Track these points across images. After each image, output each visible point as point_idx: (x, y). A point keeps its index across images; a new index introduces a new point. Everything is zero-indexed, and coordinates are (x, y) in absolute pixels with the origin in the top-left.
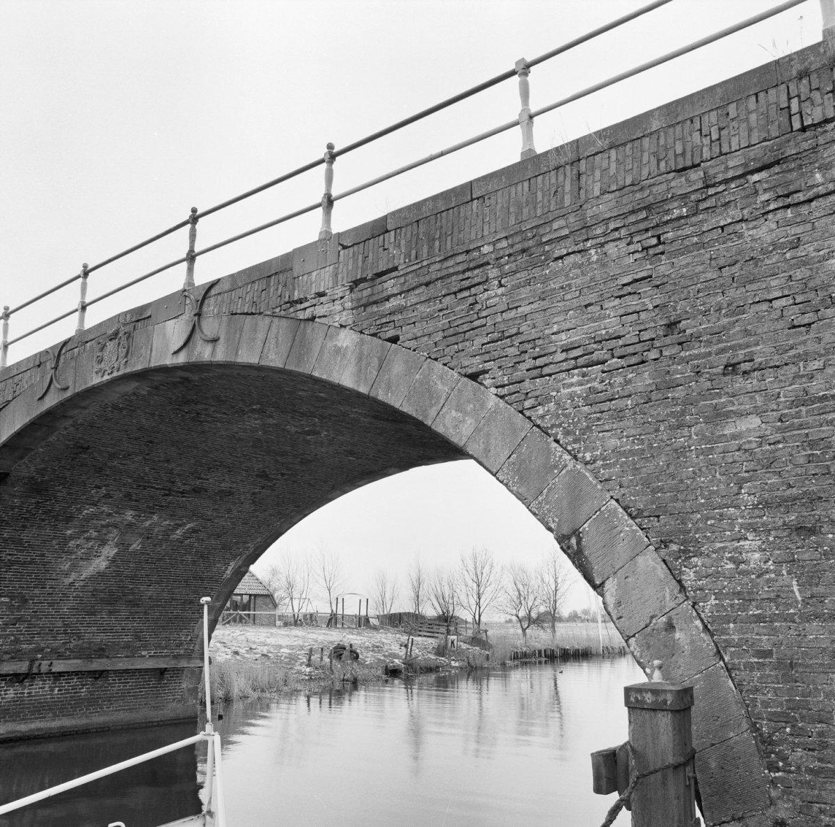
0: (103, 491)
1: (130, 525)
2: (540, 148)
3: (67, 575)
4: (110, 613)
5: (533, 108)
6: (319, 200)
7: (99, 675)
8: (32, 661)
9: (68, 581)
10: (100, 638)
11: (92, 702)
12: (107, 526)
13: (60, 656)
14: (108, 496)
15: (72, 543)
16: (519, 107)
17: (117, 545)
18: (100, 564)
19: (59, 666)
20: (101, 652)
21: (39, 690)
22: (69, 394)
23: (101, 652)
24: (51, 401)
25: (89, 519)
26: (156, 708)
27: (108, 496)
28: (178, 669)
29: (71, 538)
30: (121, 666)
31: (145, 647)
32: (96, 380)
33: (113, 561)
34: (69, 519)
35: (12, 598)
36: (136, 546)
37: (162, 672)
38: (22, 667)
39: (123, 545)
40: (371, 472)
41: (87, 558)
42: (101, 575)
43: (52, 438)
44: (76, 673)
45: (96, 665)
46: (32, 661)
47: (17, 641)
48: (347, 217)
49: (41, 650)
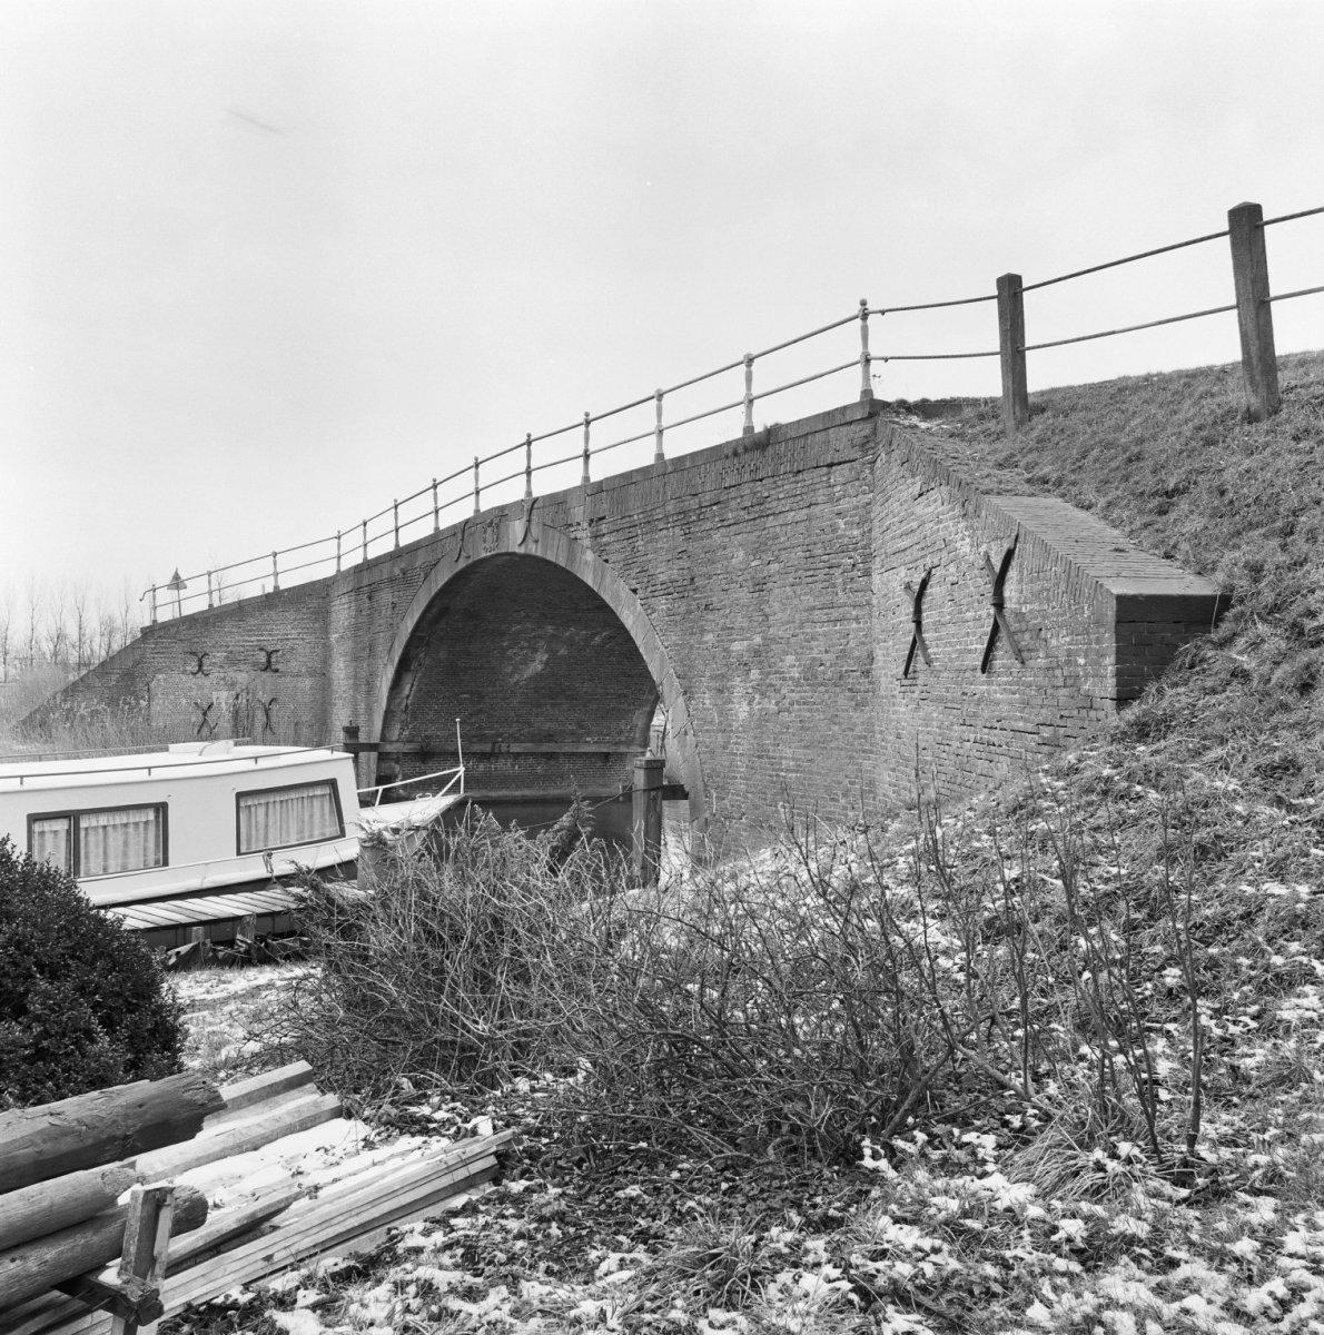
0: (522, 613)
1: (553, 636)
2: (442, 526)
3: (511, 675)
4: (553, 705)
5: (755, 393)
6: (858, 358)
7: (550, 756)
8: (494, 743)
9: (513, 681)
10: (553, 726)
11: (547, 778)
12: (534, 637)
13: (517, 740)
14: (527, 616)
15: (509, 653)
16: (744, 392)
17: (547, 652)
18: (536, 666)
19: (515, 748)
20: (550, 737)
21: (503, 766)
22: (470, 561)
23: (550, 737)
24: (462, 564)
25: (519, 632)
26: (604, 786)
27: (527, 616)
28: (621, 754)
29: (508, 648)
30: (567, 749)
31: (588, 735)
32: (484, 555)
33: (547, 664)
34: (502, 634)
35: (471, 694)
36: (563, 651)
37: (607, 755)
38: (487, 748)
39: (552, 652)
40: (437, 620)
41: (526, 661)
42: (538, 677)
43: (472, 584)
44: (532, 754)
45: (545, 748)
46: (494, 743)
47: (480, 728)
48: (601, 470)
49: (501, 735)
